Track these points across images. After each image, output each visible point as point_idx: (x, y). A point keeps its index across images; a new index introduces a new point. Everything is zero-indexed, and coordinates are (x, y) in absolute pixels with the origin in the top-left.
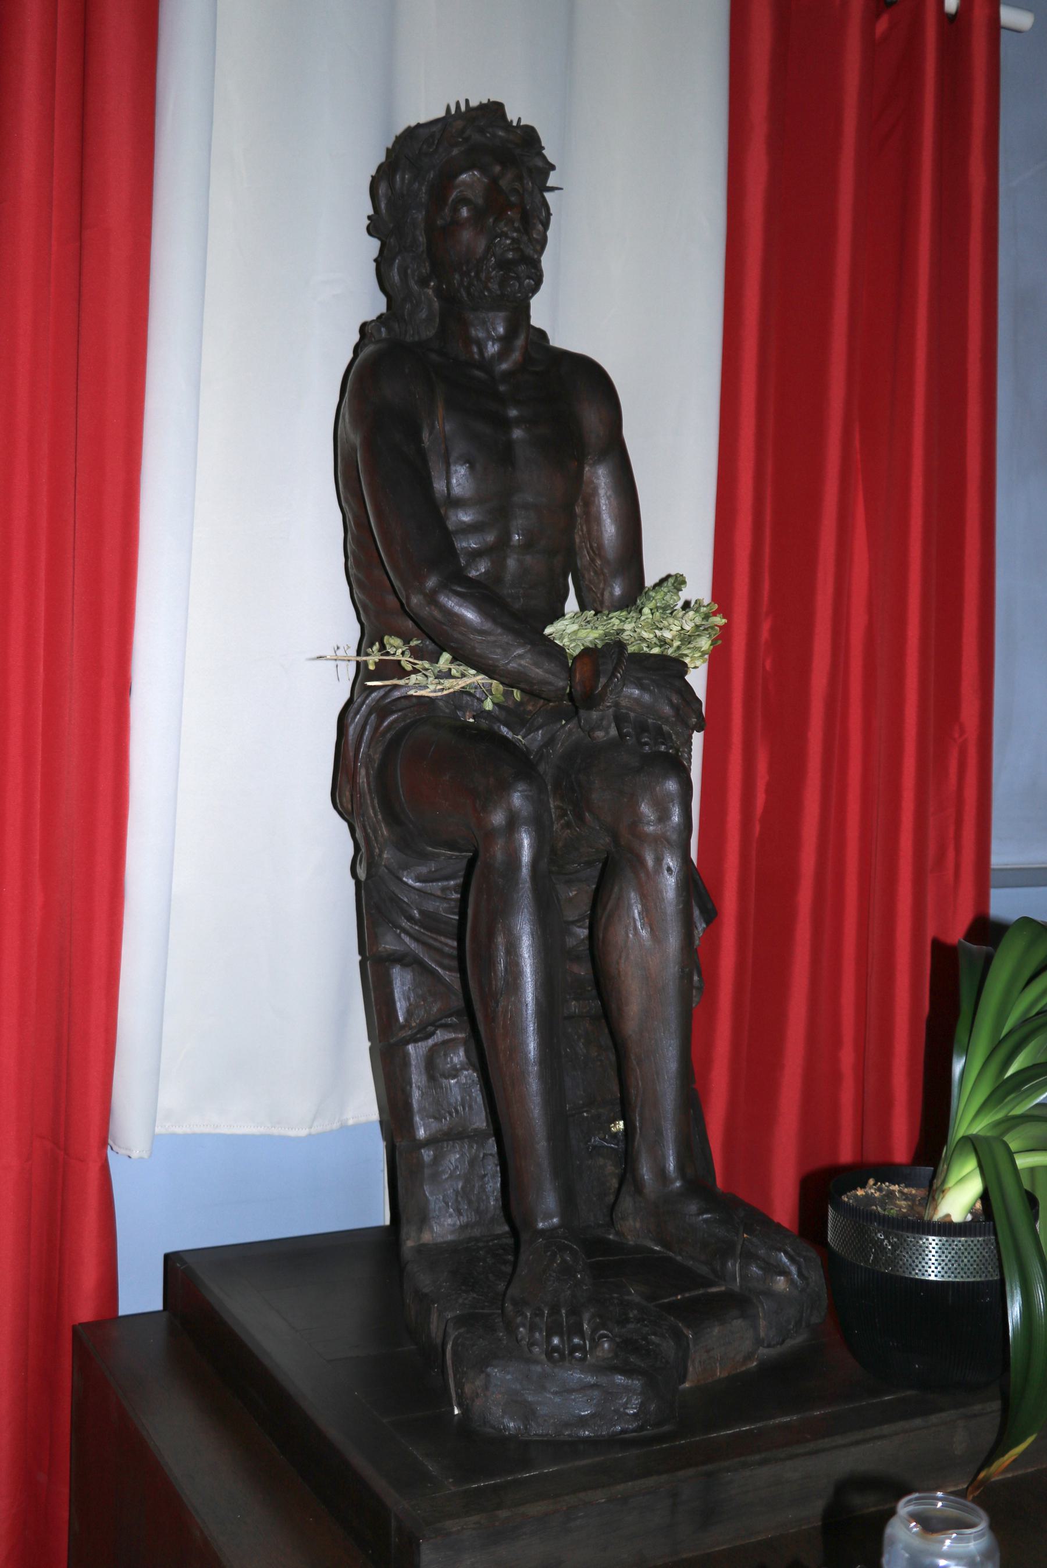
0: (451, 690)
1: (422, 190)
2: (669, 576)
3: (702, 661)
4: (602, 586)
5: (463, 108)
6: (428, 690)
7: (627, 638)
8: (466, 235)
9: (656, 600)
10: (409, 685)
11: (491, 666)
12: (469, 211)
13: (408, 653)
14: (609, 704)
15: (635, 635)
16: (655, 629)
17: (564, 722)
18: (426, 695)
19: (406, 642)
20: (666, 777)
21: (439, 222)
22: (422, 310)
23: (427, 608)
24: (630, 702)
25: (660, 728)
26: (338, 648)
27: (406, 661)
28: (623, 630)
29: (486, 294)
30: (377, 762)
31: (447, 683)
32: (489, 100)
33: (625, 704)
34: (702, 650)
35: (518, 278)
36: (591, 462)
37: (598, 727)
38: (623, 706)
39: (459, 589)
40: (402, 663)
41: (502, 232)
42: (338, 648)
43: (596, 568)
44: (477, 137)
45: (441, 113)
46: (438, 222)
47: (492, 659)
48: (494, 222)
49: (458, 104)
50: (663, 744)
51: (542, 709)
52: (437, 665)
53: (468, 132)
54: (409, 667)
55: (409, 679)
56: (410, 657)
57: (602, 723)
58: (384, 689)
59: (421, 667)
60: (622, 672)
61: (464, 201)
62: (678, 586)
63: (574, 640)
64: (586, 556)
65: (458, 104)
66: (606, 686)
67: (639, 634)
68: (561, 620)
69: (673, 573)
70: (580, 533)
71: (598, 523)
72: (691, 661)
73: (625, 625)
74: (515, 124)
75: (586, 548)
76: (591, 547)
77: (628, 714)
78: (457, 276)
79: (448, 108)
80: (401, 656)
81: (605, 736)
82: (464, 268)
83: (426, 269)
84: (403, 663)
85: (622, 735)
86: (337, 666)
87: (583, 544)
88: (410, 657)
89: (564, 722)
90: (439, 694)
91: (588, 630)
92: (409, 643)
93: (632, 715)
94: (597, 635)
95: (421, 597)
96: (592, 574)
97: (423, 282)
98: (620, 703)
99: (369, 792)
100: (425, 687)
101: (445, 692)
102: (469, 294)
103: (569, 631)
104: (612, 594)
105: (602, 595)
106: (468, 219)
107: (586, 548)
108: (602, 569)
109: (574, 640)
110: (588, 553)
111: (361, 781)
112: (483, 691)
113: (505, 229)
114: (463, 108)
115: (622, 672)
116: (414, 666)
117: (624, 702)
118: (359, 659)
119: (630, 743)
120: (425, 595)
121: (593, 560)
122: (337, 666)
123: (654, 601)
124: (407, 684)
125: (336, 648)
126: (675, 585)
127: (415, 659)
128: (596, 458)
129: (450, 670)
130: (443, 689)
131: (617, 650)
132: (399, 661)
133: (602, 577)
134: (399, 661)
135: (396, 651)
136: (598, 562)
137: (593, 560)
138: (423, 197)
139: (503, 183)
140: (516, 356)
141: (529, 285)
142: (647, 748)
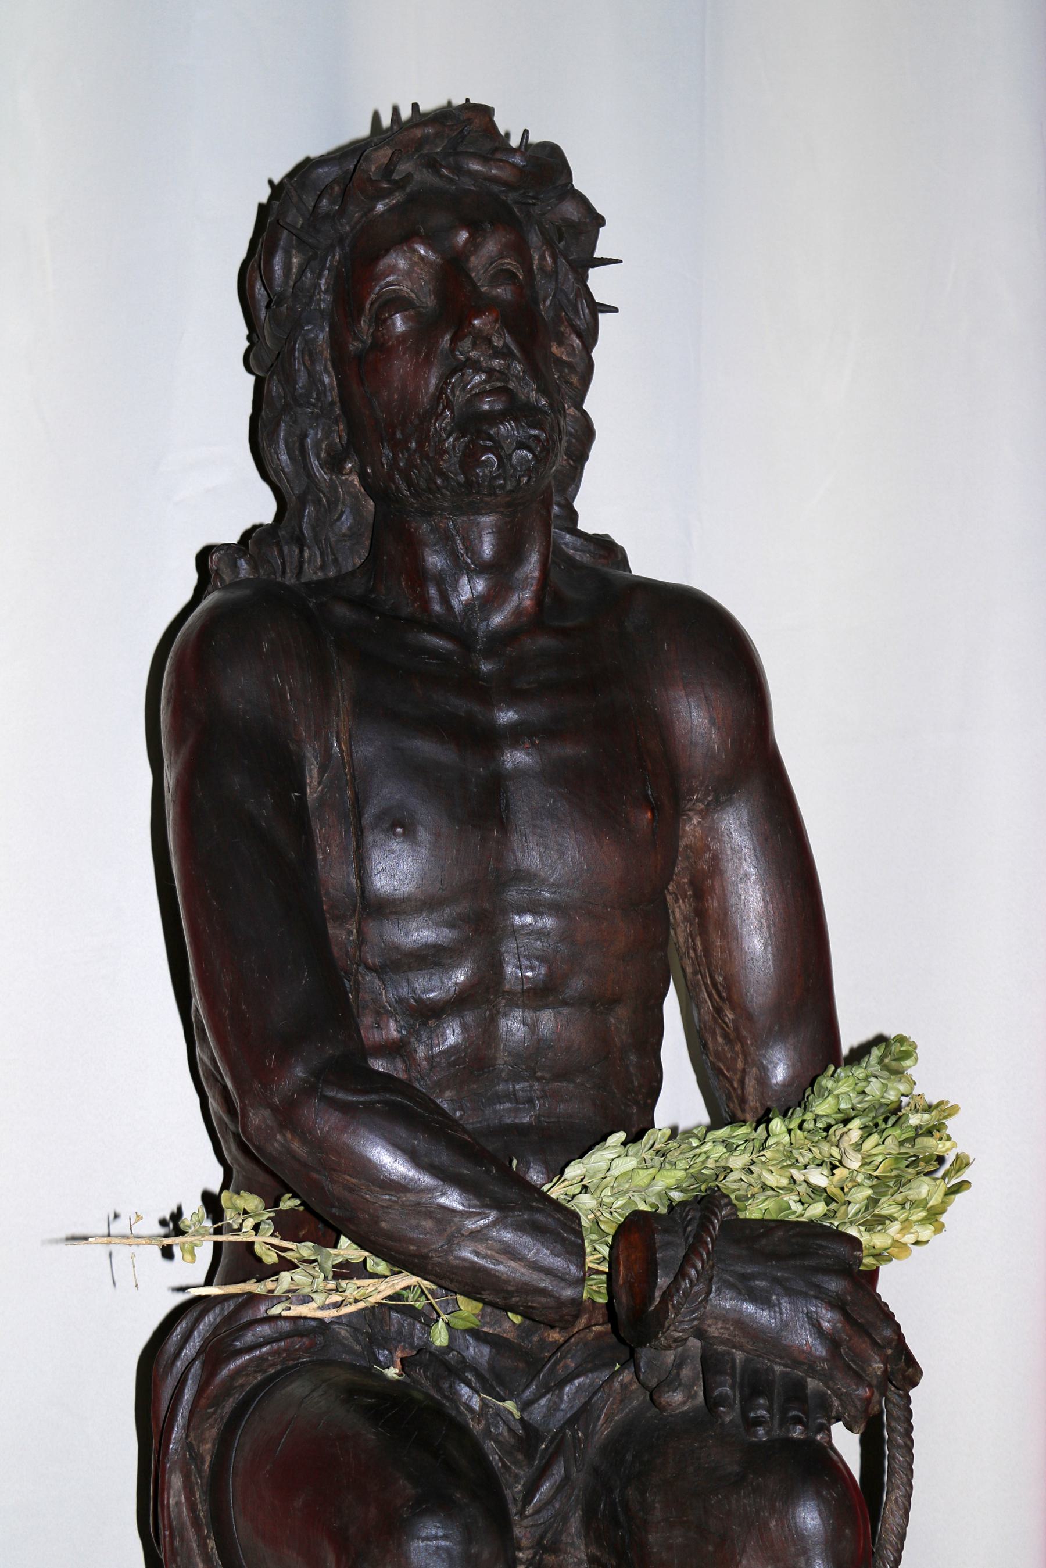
0: (361, 1305)
1: (319, 285)
2: (880, 1040)
3: (932, 1228)
4: (740, 1064)
5: (386, 121)
6: (313, 1305)
7: (734, 1186)
8: (401, 367)
9: (837, 1097)
10: (275, 1293)
11: (414, 1256)
12: (405, 320)
13: (268, 1228)
14: (677, 1335)
15: (751, 1179)
16: (792, 1165)
17: (618, 1366)
18: (309, 1315)
19: (272, 1202)
20: (790, 1498)
21: (354, 346)
22: (341, 516)
23: (278, 1137)
24: (728, 1329)
25: (799, 1386)
26: (116, 1216)
27: (267, 1243)
28: (728, 1170)
29: (439, 482)
30: (208, 1459)
31: (352, 1287)
32: (468, 100)
33: (716, 1334)
34: (930, 1204)
35: (496, 449)
36: (701, 806)
37: (671, 1381)
38: (714, 1337)
39: (341, 1096)
40: (257, 1248)
41: (468, 359)
42: (116, 1216)
43: (727, 1029)
44: (424, 177)
45: (363, 130)
46: (351, 348)
47: (412, 1241)
48: (452, 340)
49: (396, 110)
50: (798, 1421)
51: (573, 1340)
52: (332, 1251)
53: (404, 167)
54: (270, 1258)
55: (277, 1280)
56: (272, 1235)
57: (678, 1374)
58: (235, 1300)
59: (297, 1255)
60: (700, 1266)
61: (397, 303)
62: (894, 1063)
63: (624, 1192)
64: (706, 1002)
65: (396, 110)
66: (667, 1295)
67: (760, 1176)
68: (598, 1150)
69: (891, 1032)
70: (692, 954)
71: (722, 931)
72: (901, 1230)
73: (732, 1159)
74: (515, 142)
75: (705, 984)
76: (714, 984)
77: (729, 1353)
78: (387, 452)
79: (376, 118)
80: (254, 1233)
81: (684, 1403)
82: (399, 435)
83: (340, 435)
84: (258, 1249)
85: (712, 1403)
86: (110, 1255)
87: (700, 977)
88: (272, 1235)
89: (618, 1366)
90: (334, 1313)
91: (652, 1171)
92: (277, 1205)
93: (739, 1356)
94: (671, 1182)
95: (267, 1113)
96: (720, 1040)
97: (334, 464)
98: (706, 1331)
99: (192, 1524)
100: (307, 1299)
101: (345, 1310)
102: (410, 484)
103: (615, 1172)
104: (763, 1080)
105: (742, 1083)
106: (403, 338)
107: (705, 984)
108: (737, 1029)
109: (624, 1192)
110: (710, 995)
111: (172, 1502)
112: (431, 1304)
113: (474, 354)
114: (386, 121)
115: (700, 1266)
116: (282, 1254)
117: (714, 1330)
118: (219, 1238)
119: (727, 1420)
120: (274, 1109)
121: (718, 1011)
122: (110, 1255)
123: (830, 1098)
124: (272, 1291)
125: (112, 1216)
126: (887, 1061)
127: (283, 1239)
128: (710, 798)
129: (365, 1261)
130: (337, 1305)
131: (698, 1215)
132: (251, 1244)
133: (738, 1048)
134: (251, 1244)
135: (241, 1225)
136: (730, 1015)
137: (718, 1011)
138: (325, 301)
139: (477, 264)
140: (524, 597)
141: (523, 460)
142: (761, 1430)
